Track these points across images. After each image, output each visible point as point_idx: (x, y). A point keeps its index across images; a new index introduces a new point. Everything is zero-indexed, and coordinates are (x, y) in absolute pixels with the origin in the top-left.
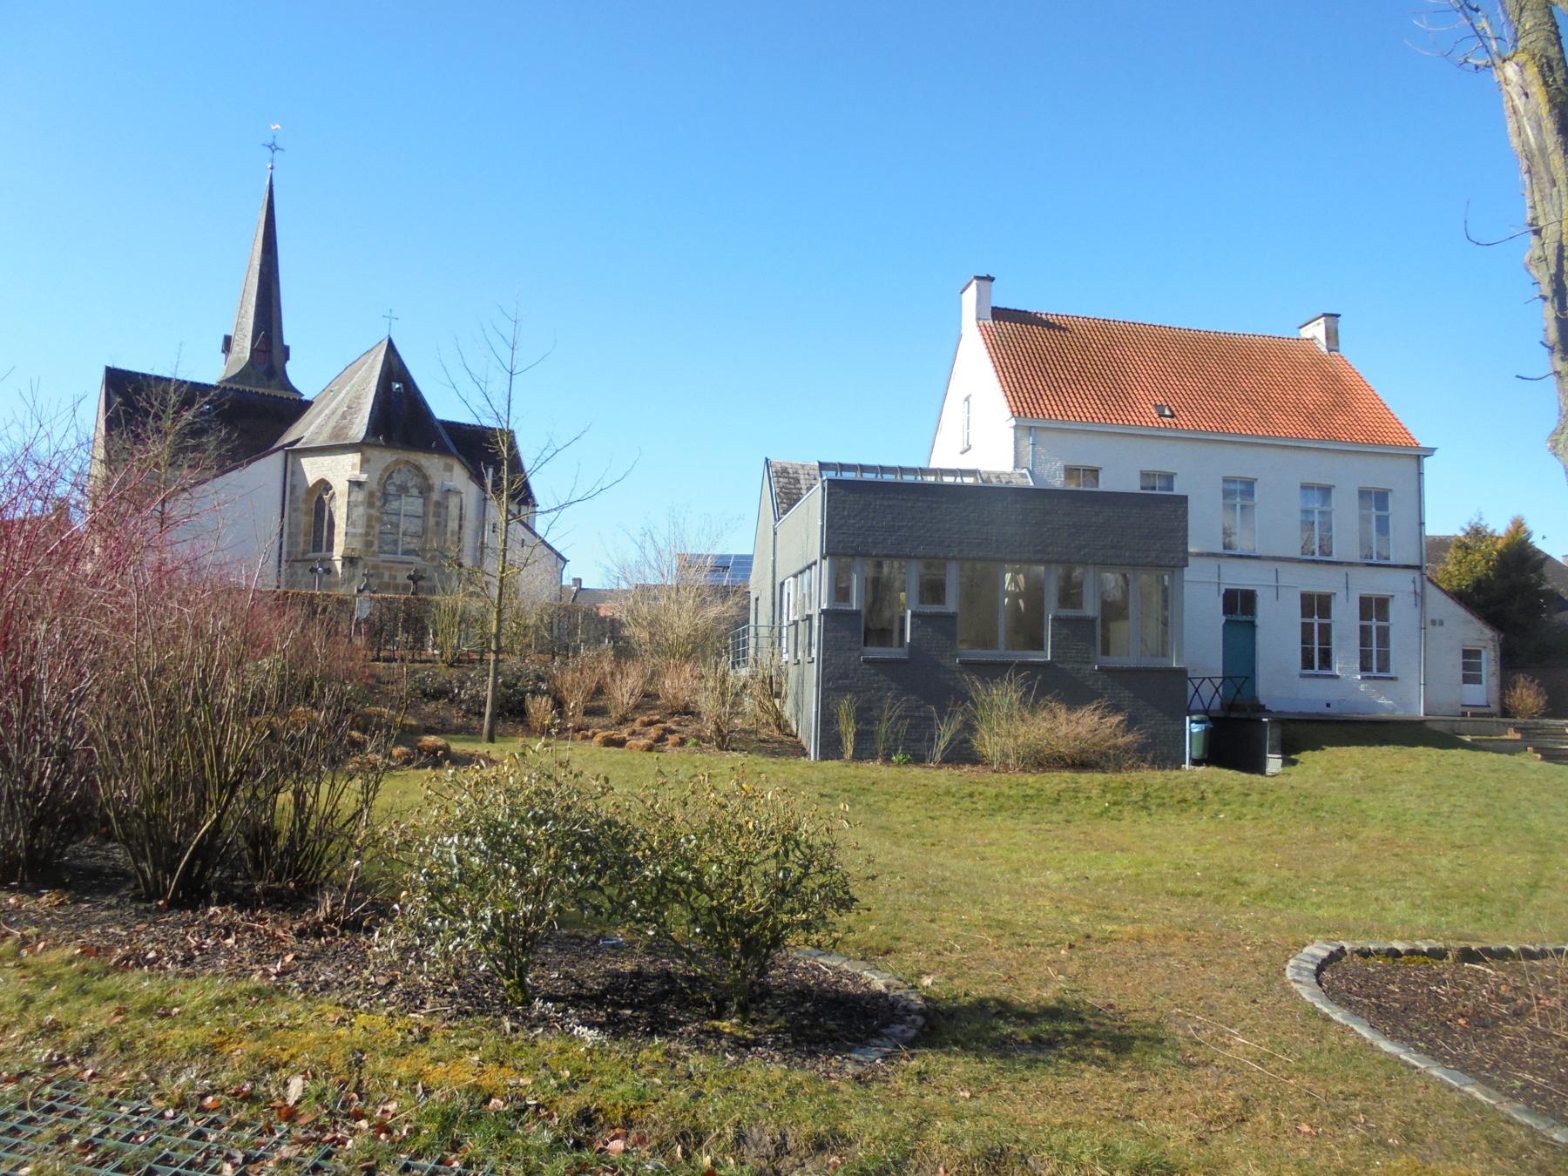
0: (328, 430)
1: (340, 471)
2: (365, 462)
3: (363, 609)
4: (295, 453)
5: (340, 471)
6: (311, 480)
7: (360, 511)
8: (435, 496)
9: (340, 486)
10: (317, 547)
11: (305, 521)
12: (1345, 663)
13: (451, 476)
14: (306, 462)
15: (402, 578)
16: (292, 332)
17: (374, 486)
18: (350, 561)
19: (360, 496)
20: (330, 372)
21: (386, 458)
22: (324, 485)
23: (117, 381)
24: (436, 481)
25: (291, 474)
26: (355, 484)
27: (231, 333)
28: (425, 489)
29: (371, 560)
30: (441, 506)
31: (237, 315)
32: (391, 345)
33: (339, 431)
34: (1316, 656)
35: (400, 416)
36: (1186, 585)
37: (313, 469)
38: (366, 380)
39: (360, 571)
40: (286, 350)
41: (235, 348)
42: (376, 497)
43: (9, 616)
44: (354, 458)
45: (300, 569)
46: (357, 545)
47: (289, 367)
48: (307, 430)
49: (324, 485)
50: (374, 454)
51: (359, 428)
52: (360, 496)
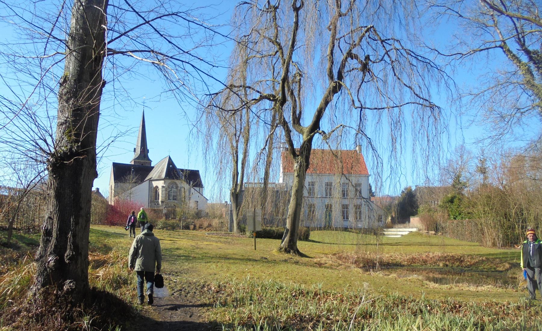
0: (157, 176)
1: (160, 184)
2: (165, 182)
3: (165, 211)
4: (151, 180)
5: (160, 184)
6: (154, 186)
7: (164, 192)
8: (179, 188)
9: (160, 187)
10: (156, 199)
11: (153, 194)
12: (351, 218)
13: (183, 185)
14: (153, 182)
15: (172, 205)
16: (149, 147)
17: (167, 187)
18: (162, 202)
19: (164, 189)
20: (157, 158)
21: (169, 181)
22: (157, 187)
23: (115, 165)
24: (179, 185)
25: (150, 185)
26: (163, 187)
27: (135, 147)
28: (177, 187)
29: (167, 202)
30: (180, 190)
31: (136, 142)
32: (170, 158)
33: (160, 176)
34: (345, 216)
35: (172, 172)
36: (90, 234)
37: (155, 184)
38: (165, 165)
39: (164, 204)
40: (148, 150)
41: (136, 151)
42: (168, 190)
43: (1, 200)
44: (163, 182)
45: (153, 204)
46: (164, 199)
47: (149, 154)
48: (153, 174)
49: (157, 187)
50: (166, 180)
51: (163, 176)
52: (164, 189)
